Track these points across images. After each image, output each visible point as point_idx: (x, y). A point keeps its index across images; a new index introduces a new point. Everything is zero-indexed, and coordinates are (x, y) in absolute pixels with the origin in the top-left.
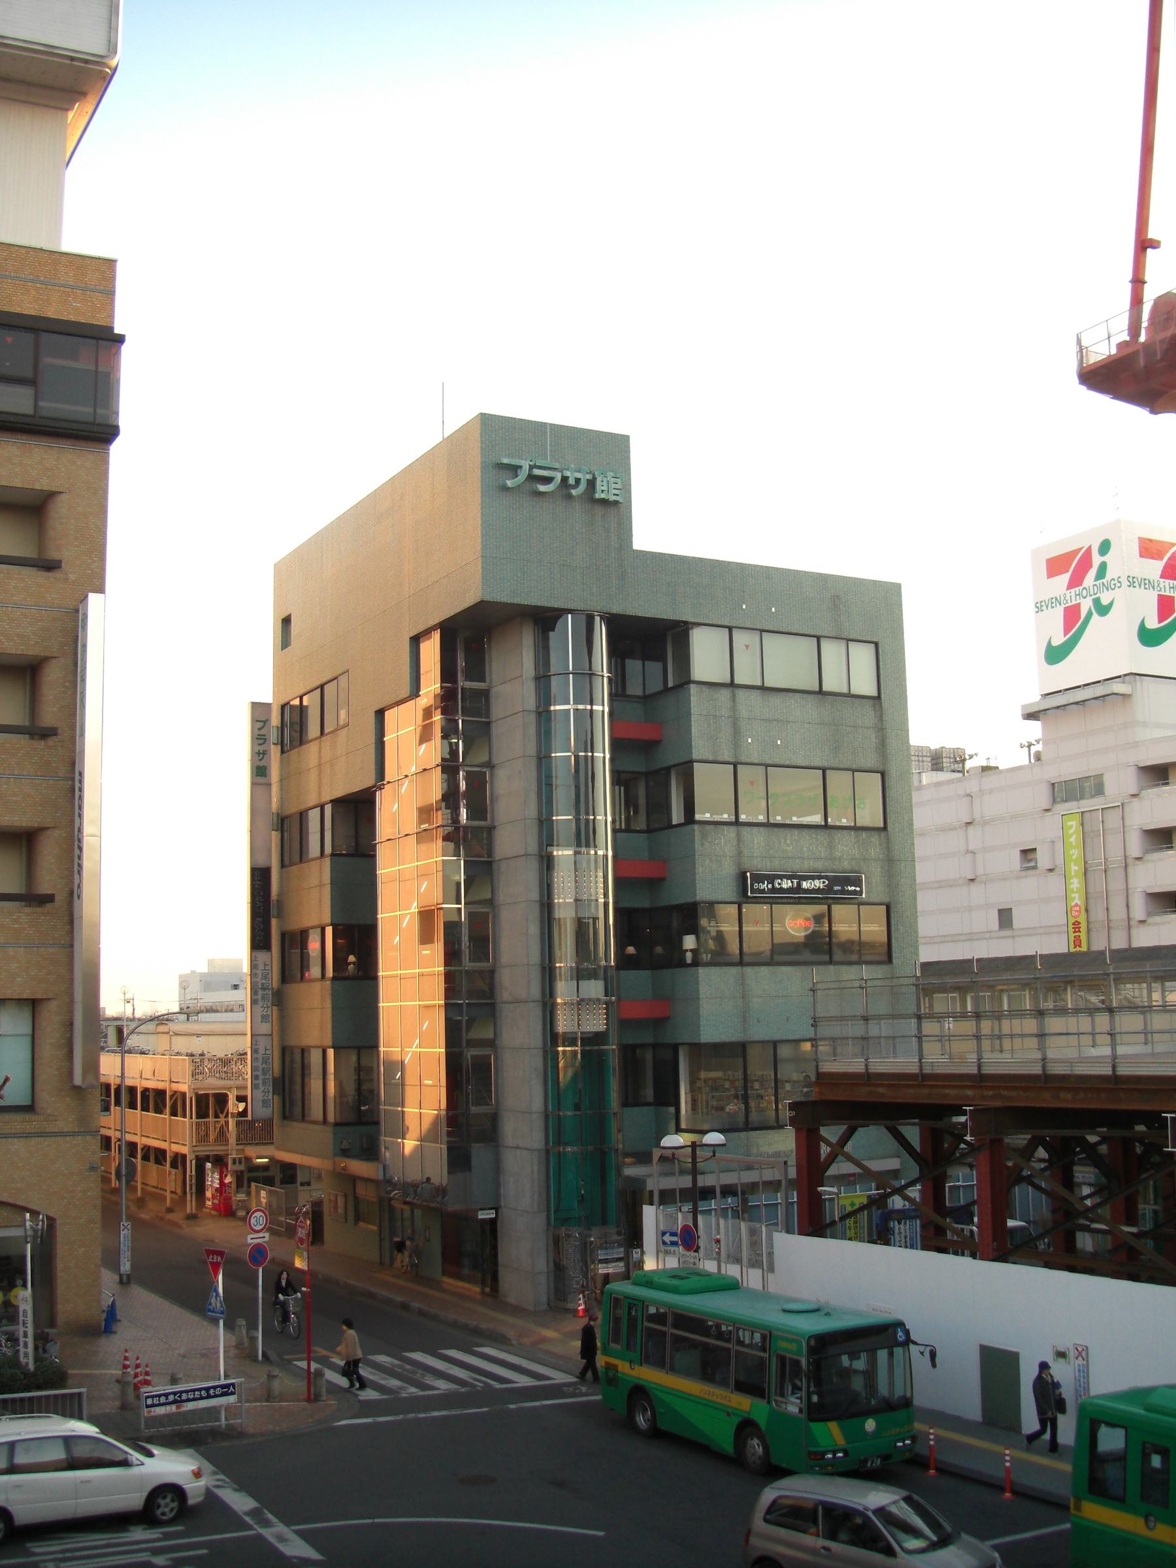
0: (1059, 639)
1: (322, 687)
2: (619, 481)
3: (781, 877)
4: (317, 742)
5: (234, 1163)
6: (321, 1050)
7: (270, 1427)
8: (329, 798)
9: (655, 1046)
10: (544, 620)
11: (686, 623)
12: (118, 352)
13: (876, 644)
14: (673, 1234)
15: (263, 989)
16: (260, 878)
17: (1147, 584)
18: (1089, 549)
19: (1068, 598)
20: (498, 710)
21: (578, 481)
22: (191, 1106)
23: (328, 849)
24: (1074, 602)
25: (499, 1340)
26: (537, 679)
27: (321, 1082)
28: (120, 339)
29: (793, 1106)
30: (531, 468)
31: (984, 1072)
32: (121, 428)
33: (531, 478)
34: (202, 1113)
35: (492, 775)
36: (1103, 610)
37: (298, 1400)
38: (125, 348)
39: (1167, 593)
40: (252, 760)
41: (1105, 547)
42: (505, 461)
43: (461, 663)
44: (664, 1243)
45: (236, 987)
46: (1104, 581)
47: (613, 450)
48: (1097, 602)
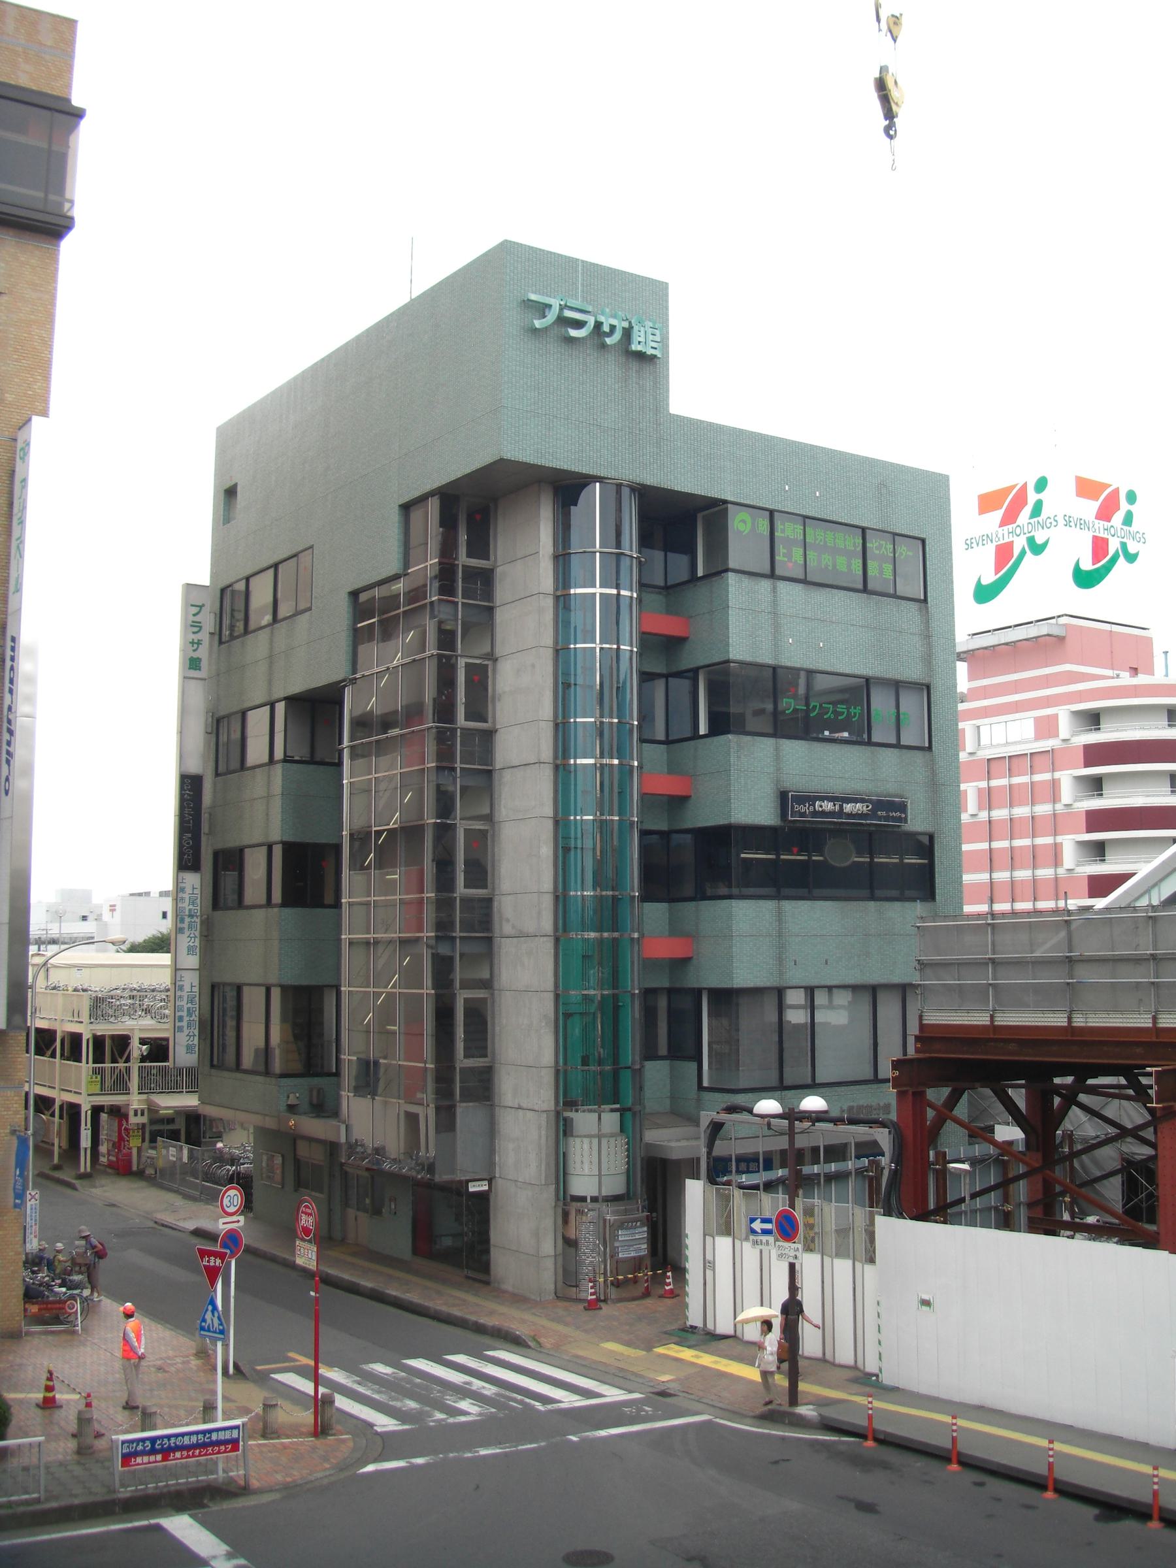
0: (989, 577)
1: (276, 566)
2: (657, 332)
3: (822, 799)
4: (268, 630)
5: (136, 1115)
6: (263, 989)
7: (279, 1477)
8: (282, 695)
9: (671, 992)
10: (567, 489)
11: (725, 502)
12: (77, 125)
13: (923, 541)
14: (764, 1221)
15: (191, 916)
16: (190, 786)
17: (1082, 524)
18: (1025, 486)
19: (1000, 536)
20: (502, 592)
21: (613, 328)
22: (87, 1050)
23: (279, 754)
24: (1006, 540)
25: (515, 1342)
26: (556, 557)
27: (263, 1027)
28: (78, 114)
29: (896, 1065)
30: (562, 308)
31: (1075, 1024)
32: (76, 220)
33: (563, 321)
34: (99, 1058)
35: (494, 670)
36: (1037, 549)
37: (302, 1435)
38: (84, 124)
39: (1101, 535)
40: (183, 651)
41: (1041, 485)
42: (533, 297)
43: (463, 537)
44: (753, 1231)
45: (84, 918)
46: (1040, 519)
47: (653, 295)
48: (1031, 541)
